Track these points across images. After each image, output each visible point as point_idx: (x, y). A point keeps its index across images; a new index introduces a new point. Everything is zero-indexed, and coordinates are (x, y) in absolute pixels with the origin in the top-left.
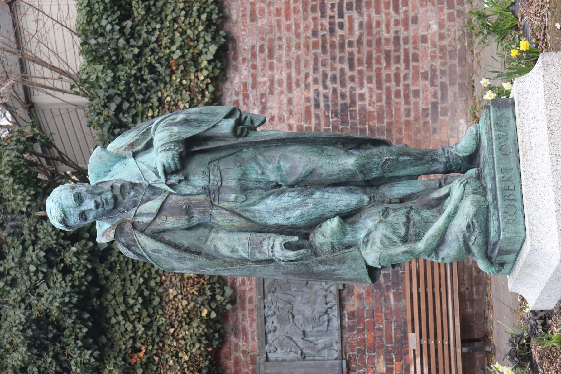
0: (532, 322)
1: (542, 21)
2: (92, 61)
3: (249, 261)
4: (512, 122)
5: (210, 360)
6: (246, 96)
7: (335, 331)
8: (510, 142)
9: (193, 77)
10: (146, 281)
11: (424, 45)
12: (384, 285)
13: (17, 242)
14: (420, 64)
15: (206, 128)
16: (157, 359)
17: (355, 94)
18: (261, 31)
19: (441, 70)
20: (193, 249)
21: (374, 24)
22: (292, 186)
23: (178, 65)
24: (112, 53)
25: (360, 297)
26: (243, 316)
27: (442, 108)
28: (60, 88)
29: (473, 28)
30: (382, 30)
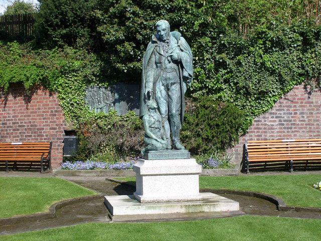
8: (176, 157)
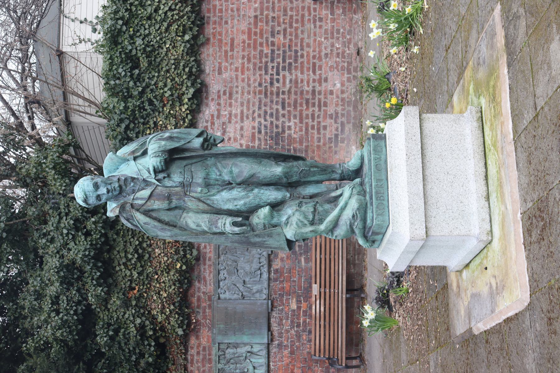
0: (391, 279)
1: (406, 86)
2: (111, 95)
3: (208, 233)
4: (384, 149)
5: (181, 297)
6: (213, 123)
7: (264, 281)
8: (382, 162)
9: (178, 109)
10: (140, 244)
11: (331, 96)
12: (298, 252)
13: (56, 214)
14: (328, 109)
15: (184, 143)
16: (145, 295)
17: (285, 126)
18: (225, 81)
19: (341, 113)
20: (171, 223)
21: (299, 81)
22: (239, 184)
23: (168, 101)
24: (125, 90)
25: (282, 260)
26: (204, 269)
27: (341, 138)
28: (89, 112)
29: (362, 87)
30: (304, 85)
